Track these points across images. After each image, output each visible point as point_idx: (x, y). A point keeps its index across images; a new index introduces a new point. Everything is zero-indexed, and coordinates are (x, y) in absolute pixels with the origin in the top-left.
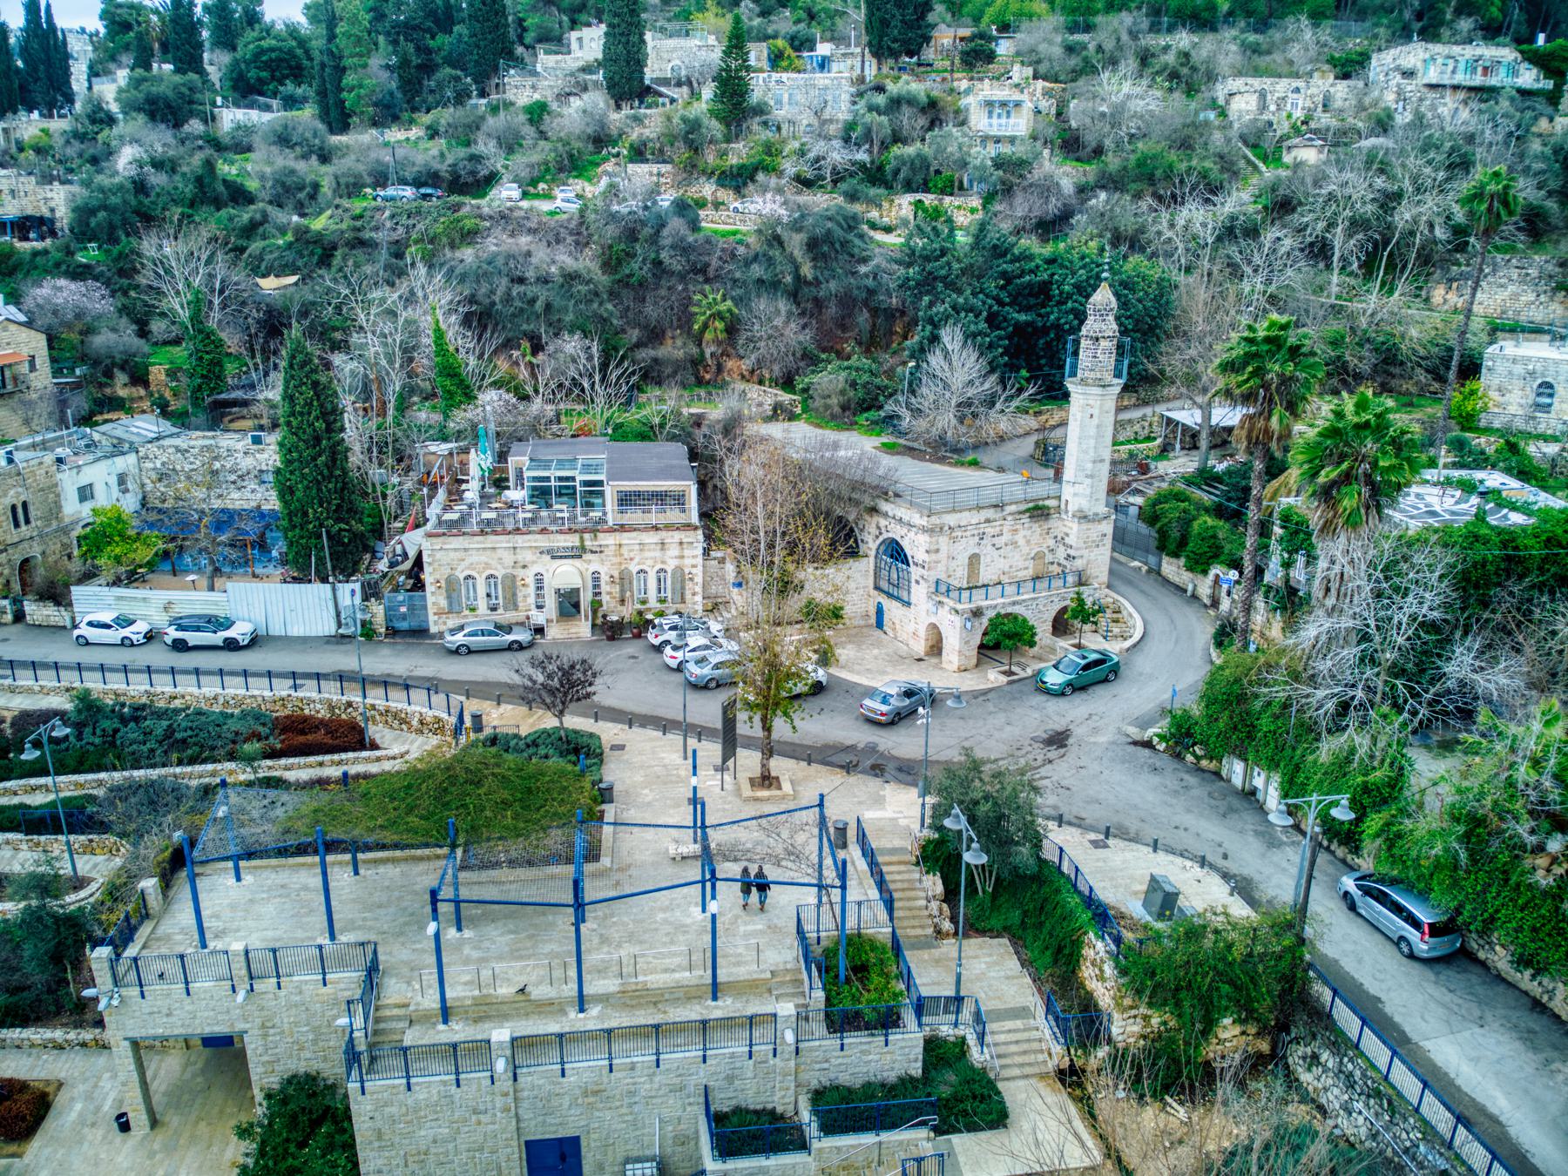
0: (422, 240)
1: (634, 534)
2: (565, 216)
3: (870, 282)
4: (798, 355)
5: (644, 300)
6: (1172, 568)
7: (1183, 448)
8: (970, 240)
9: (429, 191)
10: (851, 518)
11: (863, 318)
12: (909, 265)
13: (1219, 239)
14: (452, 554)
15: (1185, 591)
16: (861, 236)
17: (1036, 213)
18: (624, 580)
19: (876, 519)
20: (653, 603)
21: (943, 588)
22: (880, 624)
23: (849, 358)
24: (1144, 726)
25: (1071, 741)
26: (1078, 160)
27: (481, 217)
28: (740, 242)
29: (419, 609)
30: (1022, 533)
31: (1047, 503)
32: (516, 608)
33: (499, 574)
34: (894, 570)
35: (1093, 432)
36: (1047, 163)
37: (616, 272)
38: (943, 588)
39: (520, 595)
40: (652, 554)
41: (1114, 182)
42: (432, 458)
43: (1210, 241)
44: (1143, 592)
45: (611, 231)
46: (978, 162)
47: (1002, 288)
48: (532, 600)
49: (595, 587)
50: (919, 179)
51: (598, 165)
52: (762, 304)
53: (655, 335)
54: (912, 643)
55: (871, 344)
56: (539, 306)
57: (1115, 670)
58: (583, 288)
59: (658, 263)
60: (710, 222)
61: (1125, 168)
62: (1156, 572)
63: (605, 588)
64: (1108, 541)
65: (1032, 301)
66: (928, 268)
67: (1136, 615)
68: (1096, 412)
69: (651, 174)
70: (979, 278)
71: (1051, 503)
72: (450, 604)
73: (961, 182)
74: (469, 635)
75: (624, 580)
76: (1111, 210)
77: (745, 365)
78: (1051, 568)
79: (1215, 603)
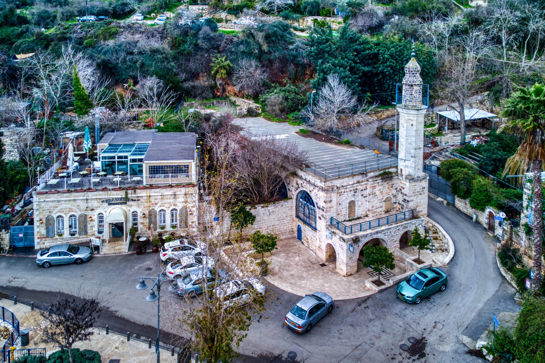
0: (92, 37)
1: (158, 190)
2: (157, 26)
3: (294, 52)
4: (261, 85)
5: (189, 61)
6: (461, 204)
7: (448, 129)
8: (339, 35)
9: (102, 17)
10: (283, 177)
11: (291, 68)
12: (312, 46)
13: (451, 35)
14: (51, 204)
15: (472, 218)
16: (290, 33)
17: (368, 24)
18: (151, 216)
19: (296, 179)
20: (168, 228)
21: (334, 223)
22: (299, 237)
23: (285, 86)
24: (475, 337)
25: (427, 350)
26: (383, 3)
27: (120, 27)
28: (235, 36)
29: (29, 235)
30: (378, 188)
31: (391, 170)
32: (86, 233)
33: (77, 215)
34: (306, 208)
35: (413, 133)
36: (370, 5)
37: (178, 49)
38: (334, 223)
39: (89, 226)
40: (169, 201)
41: (400, 12)
42: (67, 140)
43: (447, 36)
44: (448, 219)
45: (177, 32)
46: (341, 4)
47: (356, 56)
48: (96, 229)
49: (134, 220)
50: (315, 10)
51: (178, 6)
52: (244, 63)
53: (194, 76)
54: (318, 252)
55: (295, 80)
56: (138, 65)
57: (445, 284)
58: (160, 56)
59: (196, 45)
60: (222, 28)
61: (404, 7)
62: (451, 205)
63: (140, 220)
64: (426, 191)
65: (370, 61)
66: (320, 47)
67: (448, 237)
68: (414, 123)
69: (199, 9)
70: (344, 51)
71: (393, 170)
72: (48, 232)
73: (334, 12)
74: (52, 255)
75: (151, 216)
76: (401, 23)
77: (237, 89)
78: (395, 206)
79: (492, 228)
